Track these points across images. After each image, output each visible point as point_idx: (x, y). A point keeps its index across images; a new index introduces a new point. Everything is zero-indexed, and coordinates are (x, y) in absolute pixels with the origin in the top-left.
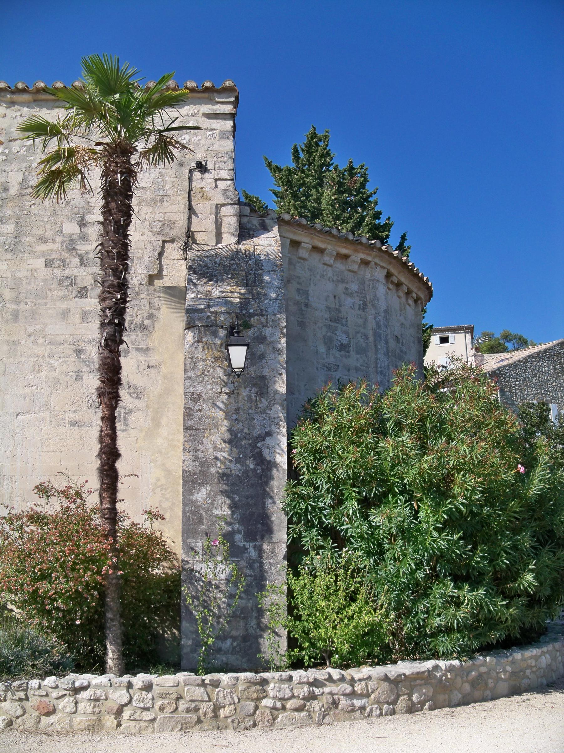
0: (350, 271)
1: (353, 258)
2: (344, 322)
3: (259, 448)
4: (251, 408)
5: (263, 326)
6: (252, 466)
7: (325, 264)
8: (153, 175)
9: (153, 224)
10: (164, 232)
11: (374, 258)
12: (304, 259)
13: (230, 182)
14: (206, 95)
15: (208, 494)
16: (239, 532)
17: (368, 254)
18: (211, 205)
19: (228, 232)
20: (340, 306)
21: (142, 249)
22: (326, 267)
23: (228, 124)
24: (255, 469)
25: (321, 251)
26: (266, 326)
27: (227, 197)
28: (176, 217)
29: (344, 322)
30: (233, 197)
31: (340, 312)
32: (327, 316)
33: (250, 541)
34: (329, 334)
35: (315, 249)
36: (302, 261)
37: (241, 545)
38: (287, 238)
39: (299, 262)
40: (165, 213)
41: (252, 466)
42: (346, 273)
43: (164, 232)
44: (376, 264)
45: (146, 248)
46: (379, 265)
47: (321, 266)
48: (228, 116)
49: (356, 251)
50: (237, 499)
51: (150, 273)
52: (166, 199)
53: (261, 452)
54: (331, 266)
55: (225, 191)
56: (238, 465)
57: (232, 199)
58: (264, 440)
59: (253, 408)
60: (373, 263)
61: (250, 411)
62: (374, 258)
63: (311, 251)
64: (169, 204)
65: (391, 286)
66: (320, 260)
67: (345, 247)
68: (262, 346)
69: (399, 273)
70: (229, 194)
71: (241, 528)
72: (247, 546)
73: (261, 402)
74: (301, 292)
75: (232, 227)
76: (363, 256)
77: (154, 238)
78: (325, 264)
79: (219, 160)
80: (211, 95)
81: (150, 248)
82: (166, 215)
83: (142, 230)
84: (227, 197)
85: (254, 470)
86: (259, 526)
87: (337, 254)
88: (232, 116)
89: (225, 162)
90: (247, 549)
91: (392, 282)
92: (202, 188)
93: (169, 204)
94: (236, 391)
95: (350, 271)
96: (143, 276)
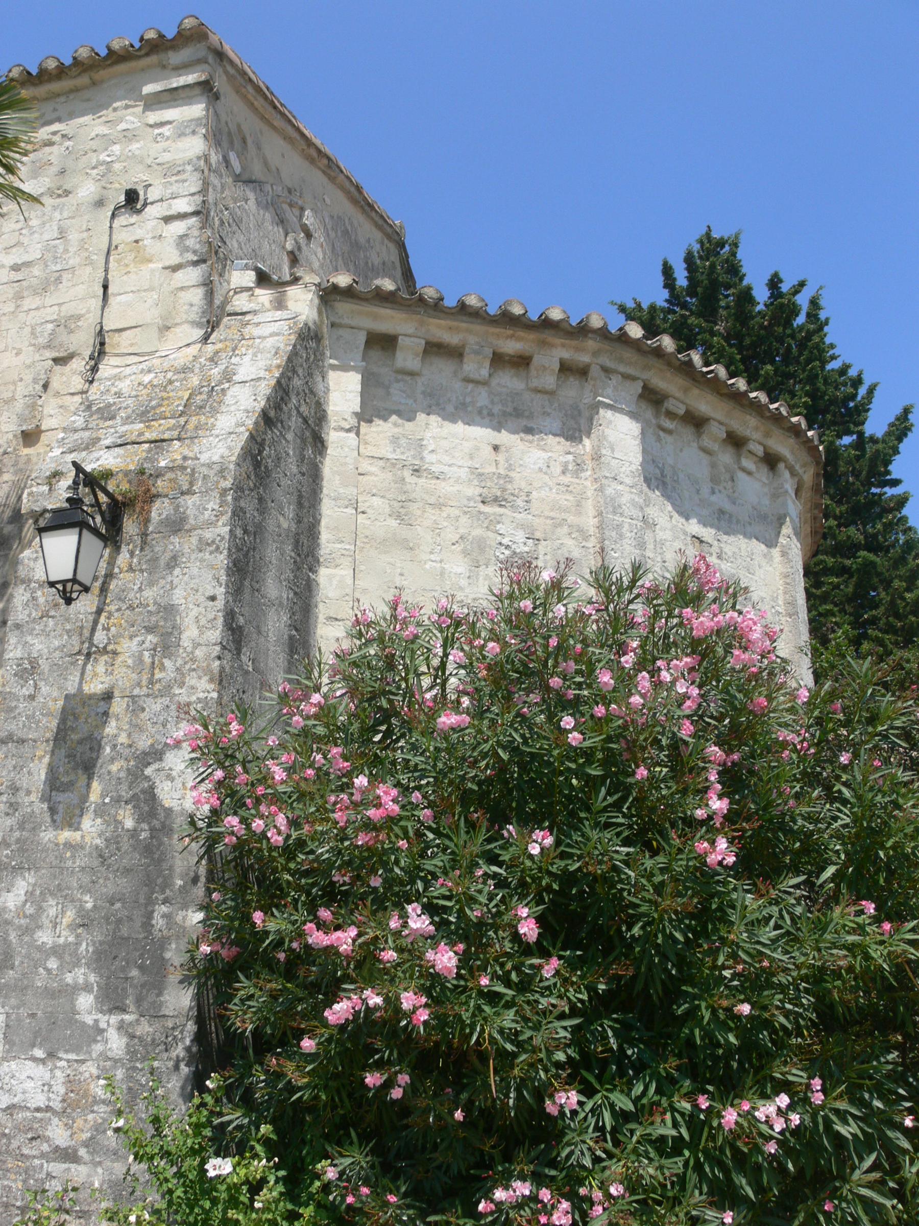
0: (537, 391)
1: (537, 360)
2: (520, 502)
3: (148, 778)
4: (139, 684)
5: (183, 493)
6: (129, 824)
7: (467, 380)
8: (46, 236)
9: (39, 329)
10: (56, 343)
11: (595, 354)
12: (412, 374)
13: (193, 220)
14: (153, 59)
15: (30, 894)
16: (87, 988)
17: (577, 349)
18: (153, 271)
19: (187, 322)
20: (510, 468)
21: (14, 383)
22: (471, 386)
23: (197, 110)
24: (135, 830)
25: (456, 353)
26: (189, 492)
27: (187, 249)
28: (81, 309)
29: (520, 502)
30: (198, 247)
31: (508, 479)
32: (473, 491)
33: (110, 1012)
34: (478, 532)
35: (434, 349)
36: (408, 378)
37: (89, 1020)
38: (359, 329)
39: (398, 381)
40: (60, 305)
41: (129, 824)
42: (527, 396)
43: (56, 343)
44: (606, 370)
45: (21, 380)
46: (615, 371)
47: (458, 385)
48: (197, 91)
49: (543, 344)
50: (89, 905)
51: (24, 428)
52: (66, 276)
53: (152, 788)
54: (485, 383)
55: (183, 237)
56: (99, 821)
57: (195, 252)
58: (161, 760)
59: (144, 683)
60: (595, 371)
61: (136, 691)
62: (595, 354)
63: (425, 352)
64: (70, 284)
65: (668, 424)
66: (455, 372)
67: (512, 336)
68: (176, 540)
69: (686, 391)
70: (190, 242)
71: (92, 978)
72: (103, 1025)
73: (163, 668)
74: (403, 441)
75: (195, 309)
76: (566, 354)
77: (37, 357)
78: (467, 380)
79: (174, 178)
80: (162, 56)
81: (28, 377)
82: (63, 308)
83: (18, 346)
84: (187, 249)
85: (134, 833)
86: (135, 973)
87: (494, 353)
88: (206, 87)
89: (184, 181)
90: (102, 1031)
91: (670, 415)
92: (137, 242)
93: (70, 284)
94: (110, 648)
95: (537, 391)
96: (10, 436)
